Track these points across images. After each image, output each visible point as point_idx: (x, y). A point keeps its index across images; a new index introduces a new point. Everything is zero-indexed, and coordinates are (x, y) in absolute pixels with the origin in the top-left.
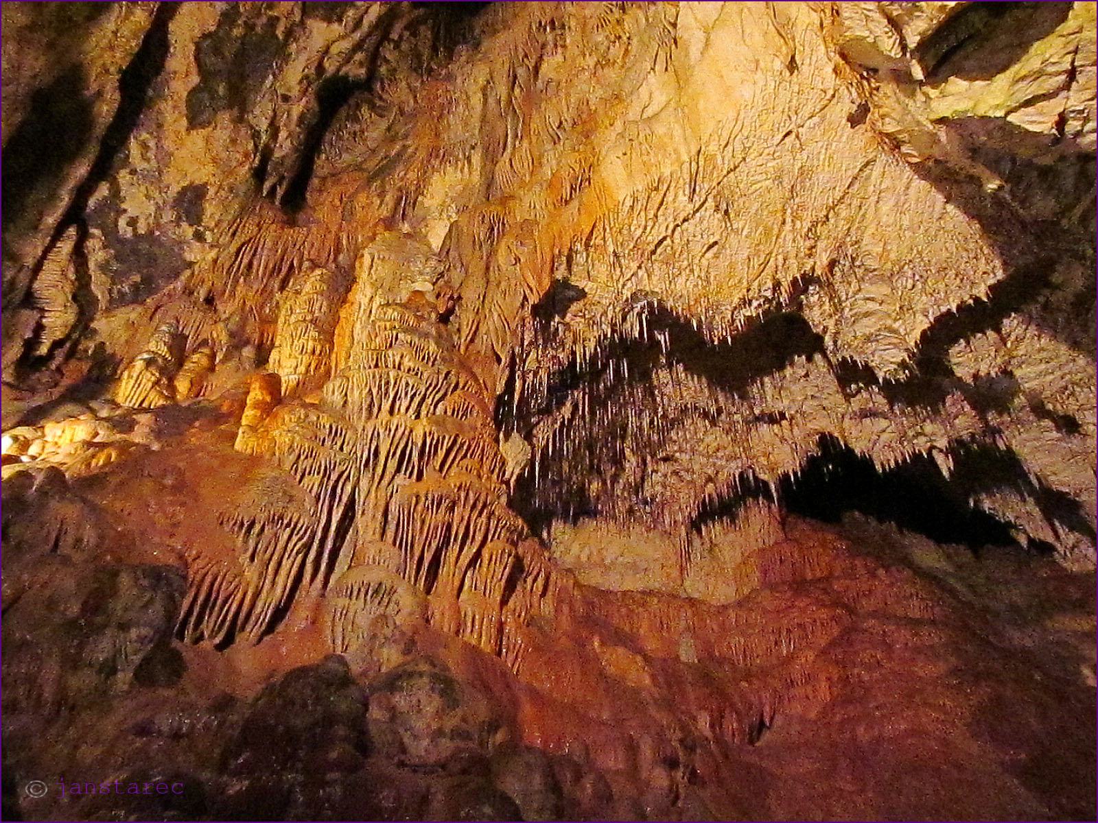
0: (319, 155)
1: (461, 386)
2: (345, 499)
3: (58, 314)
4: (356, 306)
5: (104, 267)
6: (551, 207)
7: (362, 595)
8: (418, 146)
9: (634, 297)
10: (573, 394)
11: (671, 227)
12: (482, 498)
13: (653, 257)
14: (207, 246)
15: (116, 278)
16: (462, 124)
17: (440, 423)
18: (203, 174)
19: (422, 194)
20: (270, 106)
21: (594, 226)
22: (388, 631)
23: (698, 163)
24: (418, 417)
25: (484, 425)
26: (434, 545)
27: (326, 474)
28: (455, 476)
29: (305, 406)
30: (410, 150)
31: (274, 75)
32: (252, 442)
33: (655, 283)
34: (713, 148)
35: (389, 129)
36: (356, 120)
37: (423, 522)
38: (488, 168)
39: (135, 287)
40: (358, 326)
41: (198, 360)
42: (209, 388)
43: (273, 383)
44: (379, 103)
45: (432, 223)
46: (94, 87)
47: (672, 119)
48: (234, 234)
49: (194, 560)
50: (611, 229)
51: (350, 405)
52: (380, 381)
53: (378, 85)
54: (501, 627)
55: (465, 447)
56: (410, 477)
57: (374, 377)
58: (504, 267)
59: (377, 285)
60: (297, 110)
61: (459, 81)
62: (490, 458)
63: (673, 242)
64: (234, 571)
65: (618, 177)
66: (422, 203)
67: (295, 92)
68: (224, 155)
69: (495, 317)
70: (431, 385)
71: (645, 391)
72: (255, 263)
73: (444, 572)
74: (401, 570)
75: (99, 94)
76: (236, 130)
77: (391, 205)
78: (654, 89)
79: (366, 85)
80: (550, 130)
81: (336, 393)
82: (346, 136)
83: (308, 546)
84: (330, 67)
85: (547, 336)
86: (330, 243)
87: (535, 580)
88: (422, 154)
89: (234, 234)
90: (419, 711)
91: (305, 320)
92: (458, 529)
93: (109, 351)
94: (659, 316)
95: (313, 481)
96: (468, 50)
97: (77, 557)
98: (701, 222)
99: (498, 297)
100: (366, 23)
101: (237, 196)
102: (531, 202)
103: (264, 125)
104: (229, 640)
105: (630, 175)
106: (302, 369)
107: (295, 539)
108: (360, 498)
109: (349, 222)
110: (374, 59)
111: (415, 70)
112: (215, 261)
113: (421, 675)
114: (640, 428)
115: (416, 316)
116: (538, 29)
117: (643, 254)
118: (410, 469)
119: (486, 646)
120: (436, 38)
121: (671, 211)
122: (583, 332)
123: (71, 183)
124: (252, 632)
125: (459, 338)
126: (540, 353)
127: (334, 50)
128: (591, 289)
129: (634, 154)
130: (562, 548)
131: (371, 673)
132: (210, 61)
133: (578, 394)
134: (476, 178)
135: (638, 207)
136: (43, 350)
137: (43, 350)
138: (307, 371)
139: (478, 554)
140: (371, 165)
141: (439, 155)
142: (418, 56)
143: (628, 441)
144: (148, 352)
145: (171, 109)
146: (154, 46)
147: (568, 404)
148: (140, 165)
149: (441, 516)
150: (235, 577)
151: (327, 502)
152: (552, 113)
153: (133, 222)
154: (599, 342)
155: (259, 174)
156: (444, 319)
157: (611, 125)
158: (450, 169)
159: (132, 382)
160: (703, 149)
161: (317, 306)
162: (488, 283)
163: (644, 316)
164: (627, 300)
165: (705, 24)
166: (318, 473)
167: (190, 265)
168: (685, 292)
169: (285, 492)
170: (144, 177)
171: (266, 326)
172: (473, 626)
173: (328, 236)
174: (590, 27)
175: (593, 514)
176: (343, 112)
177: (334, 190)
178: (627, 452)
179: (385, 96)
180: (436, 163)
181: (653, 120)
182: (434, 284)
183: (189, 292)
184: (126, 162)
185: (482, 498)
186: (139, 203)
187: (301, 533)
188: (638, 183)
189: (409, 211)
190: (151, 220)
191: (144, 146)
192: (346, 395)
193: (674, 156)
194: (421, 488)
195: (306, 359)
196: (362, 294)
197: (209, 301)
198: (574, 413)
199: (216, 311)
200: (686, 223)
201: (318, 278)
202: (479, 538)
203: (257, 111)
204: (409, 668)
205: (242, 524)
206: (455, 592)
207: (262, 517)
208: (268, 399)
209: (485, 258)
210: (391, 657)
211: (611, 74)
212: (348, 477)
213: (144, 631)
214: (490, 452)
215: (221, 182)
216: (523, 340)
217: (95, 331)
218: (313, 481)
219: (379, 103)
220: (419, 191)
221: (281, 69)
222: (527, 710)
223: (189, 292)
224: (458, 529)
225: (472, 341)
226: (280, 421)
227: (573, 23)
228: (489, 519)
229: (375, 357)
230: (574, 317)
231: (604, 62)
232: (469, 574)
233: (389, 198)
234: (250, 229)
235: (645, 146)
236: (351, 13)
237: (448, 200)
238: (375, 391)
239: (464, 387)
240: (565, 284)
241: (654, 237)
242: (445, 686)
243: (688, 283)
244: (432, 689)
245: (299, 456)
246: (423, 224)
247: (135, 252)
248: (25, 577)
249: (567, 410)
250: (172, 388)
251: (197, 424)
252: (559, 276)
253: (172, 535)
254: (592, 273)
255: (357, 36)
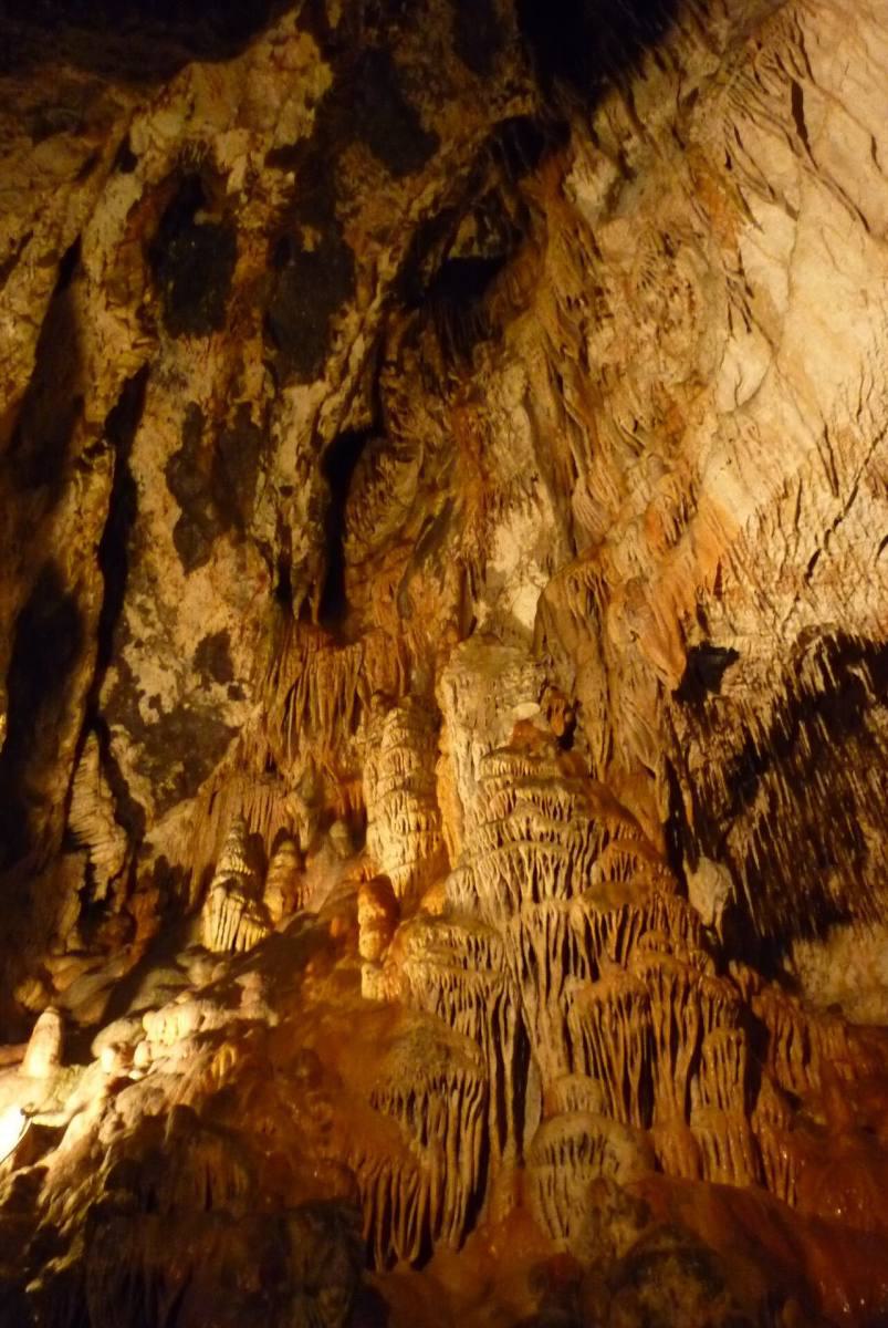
0: (346, 536)
1: (612, 835)
2: (512, 1030)
3: (105, 846)
4: (452, 759)
5: (138, 768)
6: (656, 554)
7: (567, 1157)
8: (465, 493)
9: (804, 638)
10: (764, 780)
11: (821, 536)
12: (682, 979)
13: (811, 581)
14: (248, 702)
15: (155, 775)
16: (512, 451)
17: (597, 896)
18: (221, 618)
19: (491, 558)
20: (272, 509)
21: (719, 568)
22: (611, 1201)
23: (829, 447)
24: (570, 894)
25: (656, 878)
26: (638, 1063)
27: (480, 1004)
28: (639, 963)
29: (431, 921)
30: (458, 504)
31: (264, 469)
32: (381, 984)
33: (824, 613)
34: (843, 420)
35: (422, 474)
36: (378, 476)
37: (615, 1035)
38: (563, 507)
39: (180, 778)
40: (461, 784)
41: (282, 862)
42: (306, 894)
43: (381, 887)
44: (398, 445)
45: (513, 594)
46: (72, 579)
47: (777, 398)
48: (276, 681)
49: (360, 1166)
50: (742, 564)
51: (483, 903)
52: (511, 862)
53: (392, 425)
54: (755, 1143)
55: (640, 919)
56: (583, 977)
57: (501, 859)
58: (622, 648)
59: (469, 724)
60: (304, 497)
61: (490, 398)
62: (677, 920)
63: (830, 554)
64: (408, 1166)
65: (732, 497)
66: (493, 569)
67: (295, 479)
68: (236, 587)
69: (631, 717)
70: (574, 846)
71: (860, 743)
72: (312, 709)
73: (662, 1090)
74: (606, 1108)
75: (81, 585)
76: (241, 553)
77: (455, 586)
78: (741, 360)
79: (377, 429)
80: (625, 436)
81: (462, 891)
82: (372, 502)
83: (484, 1106)
84: (327, 431)
85: (705, 721)
86: (394, 654)
87: (789, 1043)
88: (473, 507)
89: (276, 681)
90: (677, 1305)
91: (395, 789)
92: (662, 1030)
93: (172, 864)
94: (843, 649)
95: (467, 1018)
96: (489, 348)
97: (237, 1210)
98: (860, 517)
99: (627, 693)
100: (353, 364)
101: (265, 632)
102: (629, 554)
103: (270, 532)
104: (427, 1252)
105: (746, 489)
106: (411, 855)
107: (467, 1101)
108: (531, 1023)
109: (410, 618)
110: (376, 396)
111: (432, 391)
112: (264, 717)
113: (665, 1254)
114: (871, 793)
115: (529, 758)
116: (570, 307)
117: (795, 583)
118: (580, 965)
119: (741, 1180)
120: (443, 341)
121: (814, 516)
122: (750, 697)
123: (79, 693)
124: (450, 1236)
125: (593, 758)
126: (702, 742)
127: (326, 411)
128: (742, 645)
129: (742, 460)
130: (816, 976)
131: (606, 1264)
132: (191, 485)
133: (771, 777)
134: (550, 517)
135: (769, 525)
136: (101, 892)
137: (101, 892)
138: (418, 855)
139: (698, 1056)
140: (413, 532)
141: (496, 502)
142: (425, 369)
143: (861, 817)
144: (223, 873)
145: (162, 561)
146: (124, 492)
147: (762, 793)
148: (145, 633)
149: (632, 1025)
150: (412, 1173)
151: (491, 1042)
152: (626, 408)
153: (155, 702)
154: (775, 708)
155: (283, 594)
156: (566, 742)
157: (701, 423)
158: (513, 515)
159: (216, 917)
160: (830, 427)
161: (405, 764)
162: (607, 670)
163: (825, 657)
164: (794, 645)
165: (779, 257)
166: (471, 1005)
167: (235, 731)
168: (869, 612)
169: (439, 1047)
170: (153, 646)
171: (349, 787)
172: (718, 1154)
173: (390, 645)
174: (634, 286)
175: (846, 918)
176: (359, 473)
177: (382, 580)
178: (865, 827)
179: (404, 434)
180: (495, 514)
181: (752, 406)
182: (539, 701)
183: (243, 764)
184: (127, 636)
185: (682, 979)
186: (157, 680)
187: (473, 1090)
188: (758, 496)
189: (480, 584)
190: (175, 693)
191: (144, 611)
192: (475, 889)
193: (795, 447)
194: (600, 991)
195: (412, 839)
196: (454, 740)
197: (271, 767)
198: (773, 804)
199: (282, 777)
200: (840, 525)
201: (395, 723)
202: (692, 1033)
203: (258, 519)
204: (651, 1247)
205: (400, 1101)
206: (682, 1116)
207: (420, 1086)
208: (383, 912)
209: (593, 636)
210: (624, 1233)
211: (682, 338)
212: (508, 1001)
213: (334, 1291)
214: (674, 911)
215: (242, 620)
216: (674, 736)
217: (150, 847)
218: (467, 1018)
219: (398, 445)
220: (485, 555)
221: (270, 460)
222: (818, 1258)
223: (243, 764)
224: (662, 1030)
225: (610, 757)
226: (406, 949)
227: (610, 283)
228: (698, 1002)
229: (495, 832)
230: (733, 687)
231: (666, 324)
232: (694, 1084)
233: (451, 575)
234: (292, 665)
235: (753, 445)
236: (332, 363)
237: (525, 559)
238: (508, 877)
239: (616, 837)
240: (706, 648)
241: (801, 558)
242: (699, 1262)
243: (870, 599)
244: (685, 1272)
245: (441, 991)
246: (503, 596)
247: (169, 737)
248: (191, 1250)
249: (762, 804)
250: (263, 910)
251: (309, 968)
252: (695, 640)
253: (326, 1143)
254: (736, 625)
255: (348, 383)
